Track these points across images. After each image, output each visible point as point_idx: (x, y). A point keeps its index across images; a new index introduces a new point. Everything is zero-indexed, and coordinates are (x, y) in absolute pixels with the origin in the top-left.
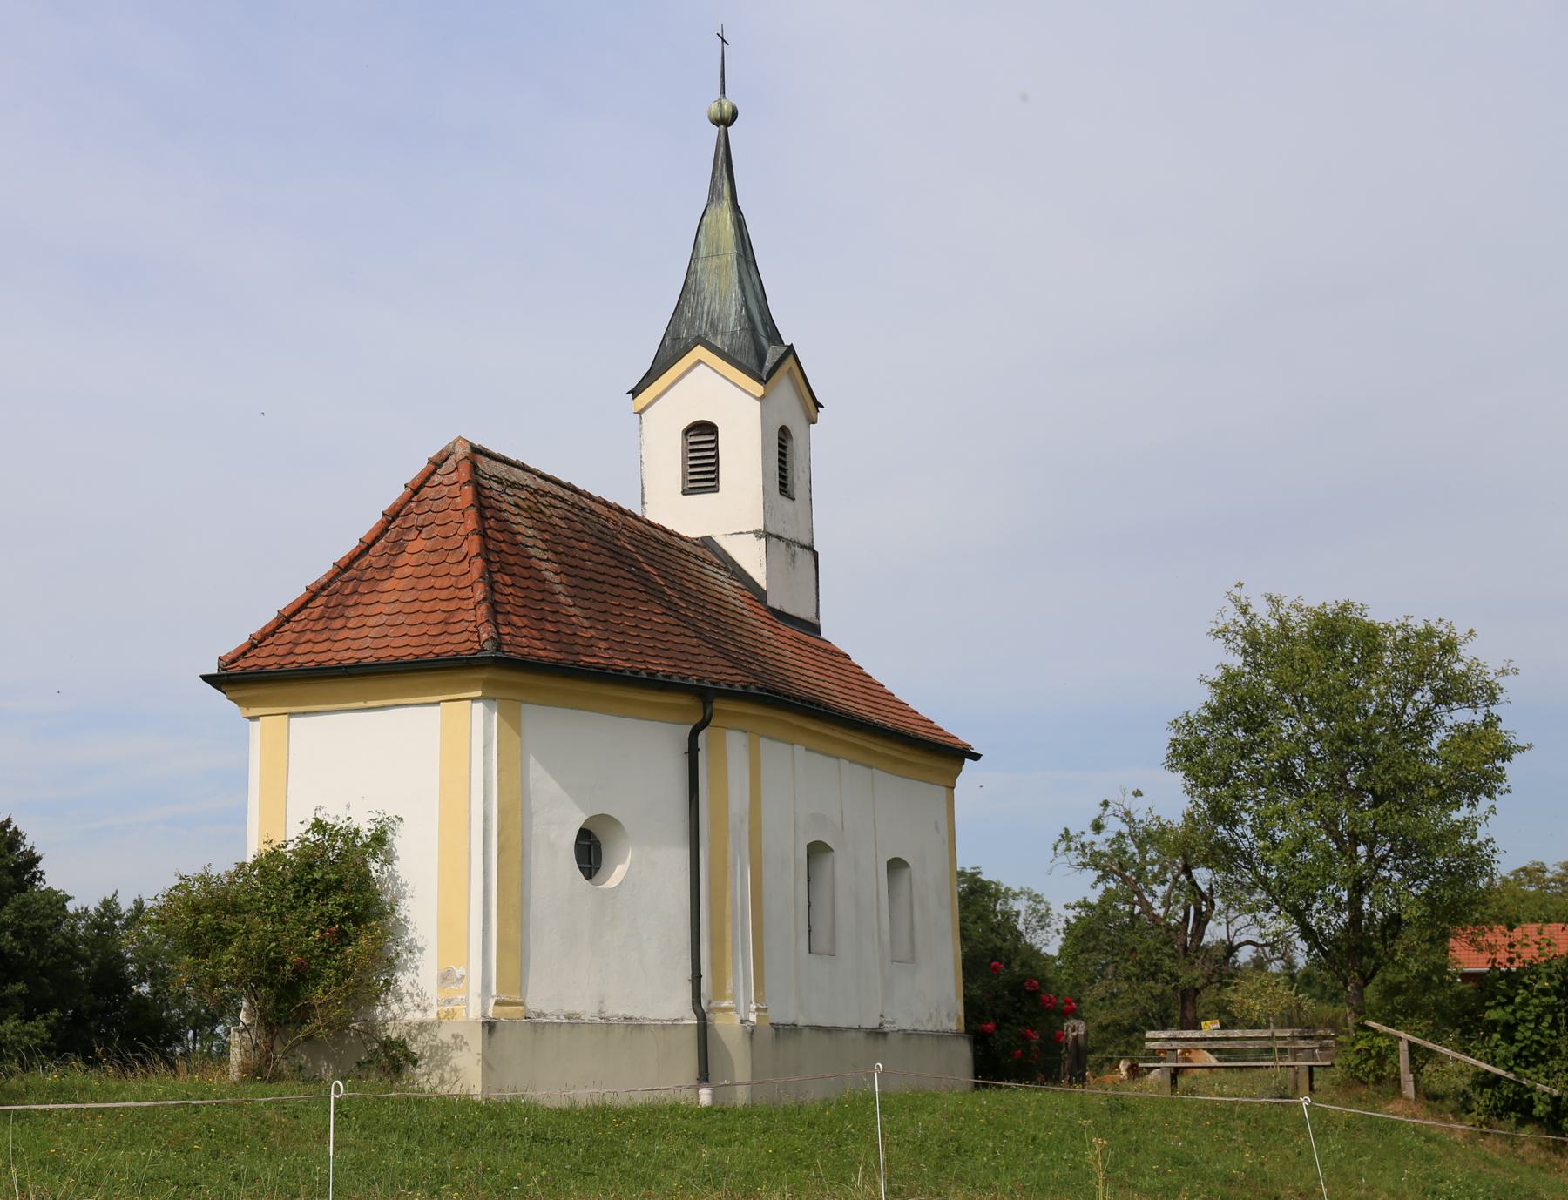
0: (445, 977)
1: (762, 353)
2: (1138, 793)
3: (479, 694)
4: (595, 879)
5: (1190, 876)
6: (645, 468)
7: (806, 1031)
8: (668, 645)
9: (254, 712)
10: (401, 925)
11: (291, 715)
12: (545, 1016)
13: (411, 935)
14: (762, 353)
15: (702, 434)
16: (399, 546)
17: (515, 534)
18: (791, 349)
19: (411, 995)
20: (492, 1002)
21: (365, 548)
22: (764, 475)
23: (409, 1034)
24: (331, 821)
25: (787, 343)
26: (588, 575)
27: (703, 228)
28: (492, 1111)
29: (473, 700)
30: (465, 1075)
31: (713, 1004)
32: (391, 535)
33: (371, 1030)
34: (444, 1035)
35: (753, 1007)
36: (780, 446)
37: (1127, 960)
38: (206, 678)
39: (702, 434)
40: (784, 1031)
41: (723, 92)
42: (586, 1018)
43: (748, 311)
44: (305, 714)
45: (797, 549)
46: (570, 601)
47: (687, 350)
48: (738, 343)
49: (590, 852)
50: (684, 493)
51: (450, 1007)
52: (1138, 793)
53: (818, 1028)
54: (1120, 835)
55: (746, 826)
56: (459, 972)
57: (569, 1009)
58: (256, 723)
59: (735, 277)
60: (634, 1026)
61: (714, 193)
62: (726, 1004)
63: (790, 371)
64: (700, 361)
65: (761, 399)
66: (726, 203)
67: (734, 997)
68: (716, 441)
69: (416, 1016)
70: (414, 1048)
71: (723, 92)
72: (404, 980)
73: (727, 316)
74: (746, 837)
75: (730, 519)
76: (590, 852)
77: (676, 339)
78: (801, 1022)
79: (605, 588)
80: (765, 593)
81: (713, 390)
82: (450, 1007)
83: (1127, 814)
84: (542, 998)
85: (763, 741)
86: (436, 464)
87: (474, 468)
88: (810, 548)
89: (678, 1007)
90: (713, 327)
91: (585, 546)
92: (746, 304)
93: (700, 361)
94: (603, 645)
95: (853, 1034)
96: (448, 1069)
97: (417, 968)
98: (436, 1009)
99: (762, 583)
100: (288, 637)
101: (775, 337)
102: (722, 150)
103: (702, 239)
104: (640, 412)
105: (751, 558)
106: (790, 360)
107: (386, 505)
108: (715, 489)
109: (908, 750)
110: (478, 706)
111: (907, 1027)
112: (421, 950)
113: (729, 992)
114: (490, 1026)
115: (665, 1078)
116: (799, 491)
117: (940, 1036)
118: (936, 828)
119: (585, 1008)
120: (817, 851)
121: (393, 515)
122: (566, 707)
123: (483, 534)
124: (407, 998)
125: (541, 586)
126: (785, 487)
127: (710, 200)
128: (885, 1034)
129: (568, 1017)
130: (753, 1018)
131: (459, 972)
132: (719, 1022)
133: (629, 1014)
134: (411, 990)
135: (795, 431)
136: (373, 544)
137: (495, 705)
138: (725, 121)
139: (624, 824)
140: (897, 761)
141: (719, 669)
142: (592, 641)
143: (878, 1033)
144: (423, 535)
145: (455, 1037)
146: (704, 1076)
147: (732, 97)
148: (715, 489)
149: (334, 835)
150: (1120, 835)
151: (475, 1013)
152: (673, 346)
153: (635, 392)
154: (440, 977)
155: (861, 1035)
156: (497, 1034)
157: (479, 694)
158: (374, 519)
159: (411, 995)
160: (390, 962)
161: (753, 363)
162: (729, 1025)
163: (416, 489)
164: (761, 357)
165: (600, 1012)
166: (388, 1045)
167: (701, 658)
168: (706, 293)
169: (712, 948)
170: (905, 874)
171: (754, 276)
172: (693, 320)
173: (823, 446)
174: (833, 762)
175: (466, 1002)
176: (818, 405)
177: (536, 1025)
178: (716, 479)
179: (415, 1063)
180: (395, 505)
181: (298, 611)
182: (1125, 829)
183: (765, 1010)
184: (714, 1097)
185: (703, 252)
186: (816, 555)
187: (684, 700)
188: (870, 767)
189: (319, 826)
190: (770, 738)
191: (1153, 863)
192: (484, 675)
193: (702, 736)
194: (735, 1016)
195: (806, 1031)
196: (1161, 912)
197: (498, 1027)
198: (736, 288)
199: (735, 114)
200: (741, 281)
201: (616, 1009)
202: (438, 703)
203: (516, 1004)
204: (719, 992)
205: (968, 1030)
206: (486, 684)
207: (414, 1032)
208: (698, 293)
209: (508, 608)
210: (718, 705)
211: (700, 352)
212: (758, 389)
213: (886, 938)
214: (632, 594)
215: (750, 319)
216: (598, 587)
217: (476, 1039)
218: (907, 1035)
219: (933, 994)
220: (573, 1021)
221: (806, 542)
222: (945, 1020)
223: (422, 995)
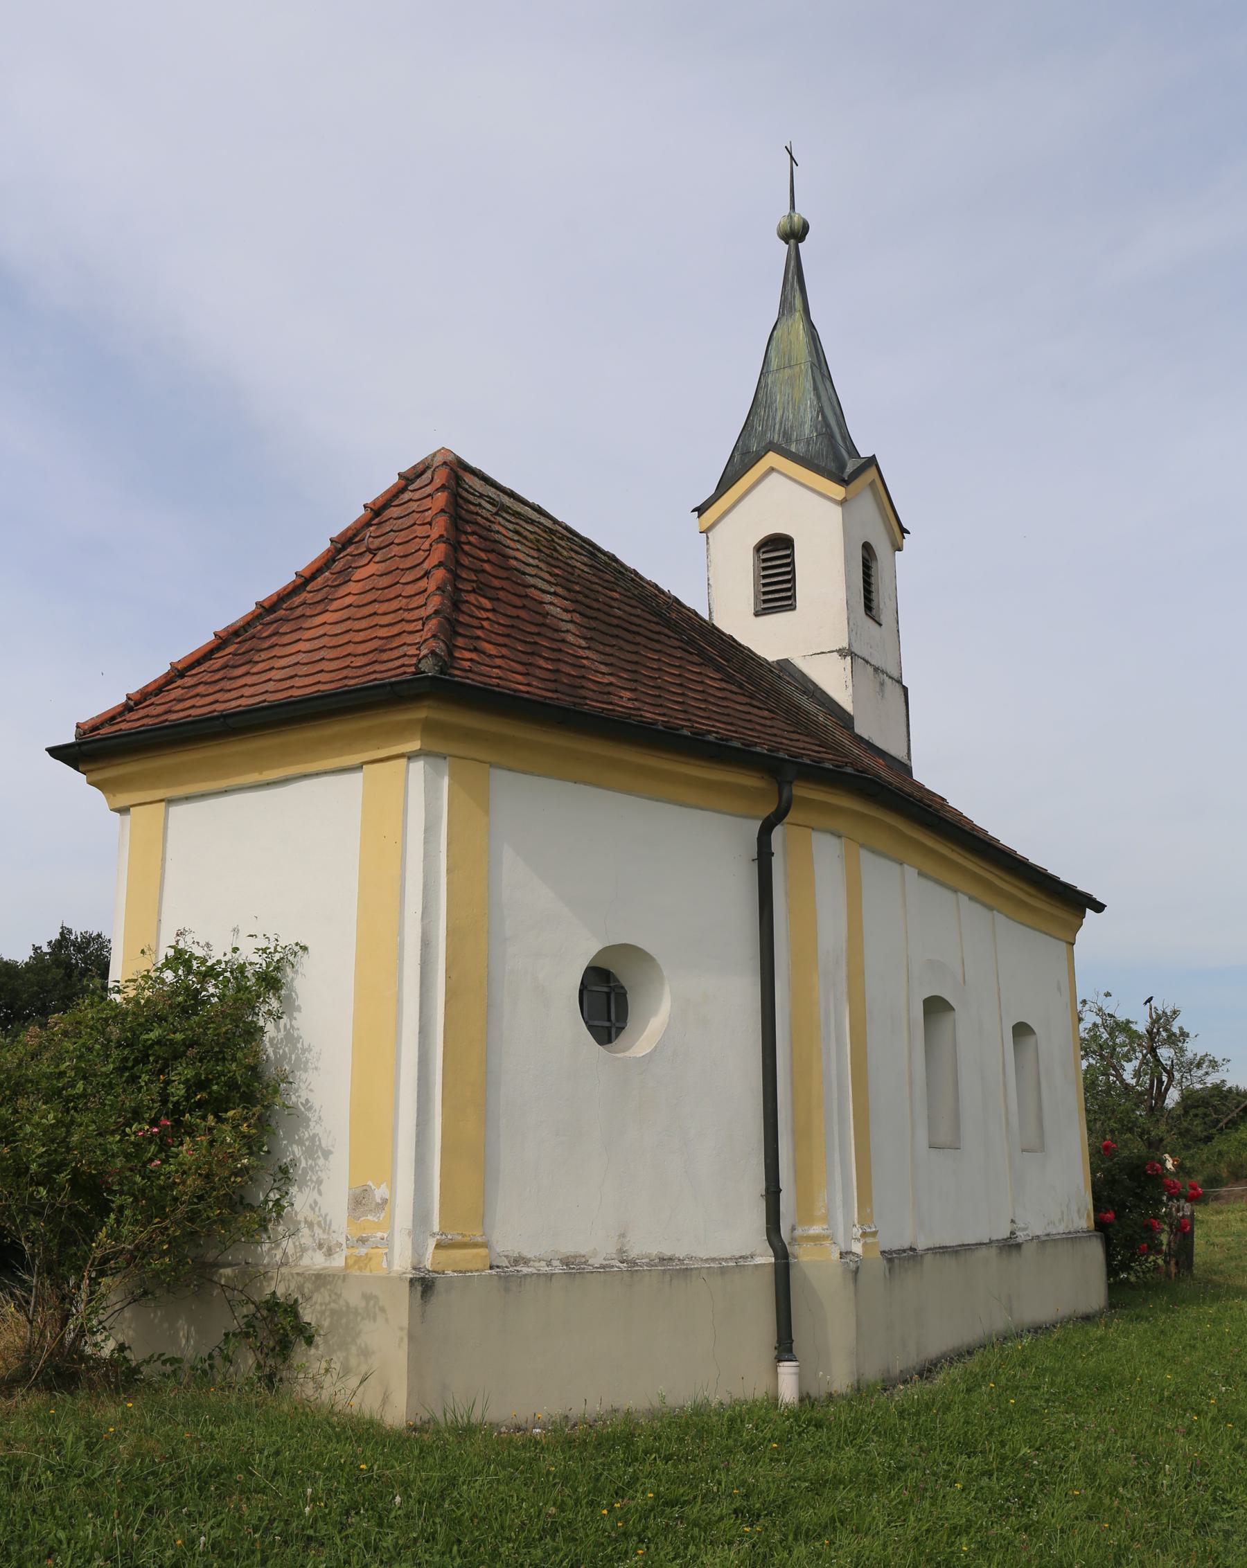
0: (360, 1201)
1: (839, 461)
2: (1108, 995)
3: (415, 745)
4: (617, 1043)
5: (1155, 1056)
6: (713, 590)
7: (929, 1258)
8: (726, 711)
9: (124, 799)
10: (297, 1117)
11: (170, 801)
12: (526, 1262)
13: (314, 1128)
14: (839, 461)
15: (776, 554)
16: (345, 576)
17: (507, 557)
18: (872, 461)
19: (310, 1225)
20: (432, 1243)
21: (304, 581)
22: (848, 588)
23: (300, 1288)
24: (199, 952)
25: (865, 453)
26: (615, 621)
27: (774, 343)
28: (420, 1441)
29: (410, 757)
30: (372, 1374)
31: (799, 1232)
32: (337, 566)
33: (253, 1274)
34: (352, 1296)
35: (857, 1232)
36: (864, 573)
37: (1110, 1119)
38: (55, 752)
39: (776, 554)
40: (900, 1260)
41: (793, 207)
42: (597, 1261)
43: (824, 417)
44: (187, 799)
45: (887, 679)
46: (583, 643)
47: (758, 457)
48: (814, 448)
49: (606, 1000)
50: (757, 614)
51: (363, 1251)
52: (1108, 995)
53: (942, 1251)
54: (1095, 1025)
55: (843, 972)
56: (380, 1192)
57: (569, 1247)
58: (127, 818)
59: (809, 385)
60: (673, 1270)
61: (786, 307)
62: (816, 1230)
63: (872, 484)
64: (772, 469)
65: (842, 503)
66: (798, 315)
67: (828, 1218)
68: (791, 556)
69: (315, 1261)
70: (308, 1315)
71: (793, 207)
72: (301, 1201)
73: (802, 424)
74: (843, 987)
75: (806, 639)
76: (606, 1000)
77: (746, 453)
78: (921, 1245)
79: (639, 639)
80: (851, 718)
81: (789, 501)
82: (363, 1251)
83: (1100, 1009)
84: (525, 1229)
85: (865, 855)
86: (408, 479)
87: (458, 479)
88: (899, 682)
89: (743, 1236)
90: (786, 435)
91: (616, 595)
92: (821, 410)
93: (772, 469)
94: (628, 694)
95: (983, 1252)
96: (354, 1350)
97: (319, 1182)
98: (345, 1252)
99: (848, 706)
100: (177, 693)
101: (853, 452)
102: (792, 263)
103: (772, 354)
104: (706, 532)
105: (834, 680)
106: (871, 474)
107: (337, 530)
108: (792, 607)
109: (1032, 891)
110: (418, 767)
111: (1039, 1232)
112: (327, 1154)
113: (820, 1211)
114: (424, 1285)
115: (717, 1364)
116: (885, 617)
117: (1072, 1238)
118: (1059, 989)
119: (597, 1246)
120: (935, 1007)
121: (344, 543)
122: (563, 778)
123: (455, 546)
124: (305, 1231)
125: (540, 619)
126: (869, 607)
127: (781, 314)
128: (1019, 1246)
129: (566, 1262)
130: (857, 1248)
131: (380, 1192)
132: (803, 1256)
133: (668, 1253)
134: (311, 1217)
135: (881, 547)
136: (313, 577)
137: (444, 766)
138: (795, 234)
139: (660, 960)
140: (1022, 904)
141: (801, 745)
142: (611, 689)
143: (1010, 1246)
144: (377, 559)
145: (367, 1297)
146: (785, 1347)
147: (802, 211)
148: (792, 607)
149: (211, 973)
150: (1095, 1025)
151: (401, 1261)
152: (742, 460)
153: (700, 510)
154: (356, 1195)
155: (993, 1251)
156: (439, 1298)
157: (415, 745)
158: (321, 546)
159: (310, 1225)
160: (284, 1171)
161: (832, 466)
162: (817, 1262)
163: (377, 511)
164: (842, 466)
165: (621, 1251)
166: (272, 1305)
167: (775, 731)
168: (778, 404)
169: (796, 1147)
170: (1030, 1041)
171: (828, 383)
172: (764, 433)
173: (908, 572)
174: (949, 895)
175: (388, 1242)
176: (904, 531)
177: (509, 1277)
178: (793, 597)
179: (310, 1341)
180: (349, 529)
181: (191, 666)
182: (1099, 1021)
183: (874, 1234)
184: (801, 1378)
185: (774, 364)
186: (905, 690)
187: (750, 780)
188: (990, 908)
189: (180, 959)
190: (873, 851)
191: (1123, 1045)
192: (421, 713)
193: (777, 834)
194: (832, 1235)
195: (929, 1258)
196: (1133, 1082)
197: (440, 1286)
198: (811, 395)
199: (805, 228)
200: (816, 389)
201: (644, 1246)
202: (358, 768)
203: (476, 1245)
204: (806, 1215)
205: (1100, 1226)
206: (429, 729)
207: (308, 1286)
208: (769, 406)
209: (479, 633)
210: (801, 791)
211: (772, 459)
212: (838, 491)
213: (1015, 1120)
214: (679, 653)
215: (828, 425)
216: (629, 637)
217: (400, 1306)
218: (1044, 1242)
219: (1060, 1192)
220: (574, 1267)
221: (896, 675)
222: (1075, 1217)
223: (326, 1226)
